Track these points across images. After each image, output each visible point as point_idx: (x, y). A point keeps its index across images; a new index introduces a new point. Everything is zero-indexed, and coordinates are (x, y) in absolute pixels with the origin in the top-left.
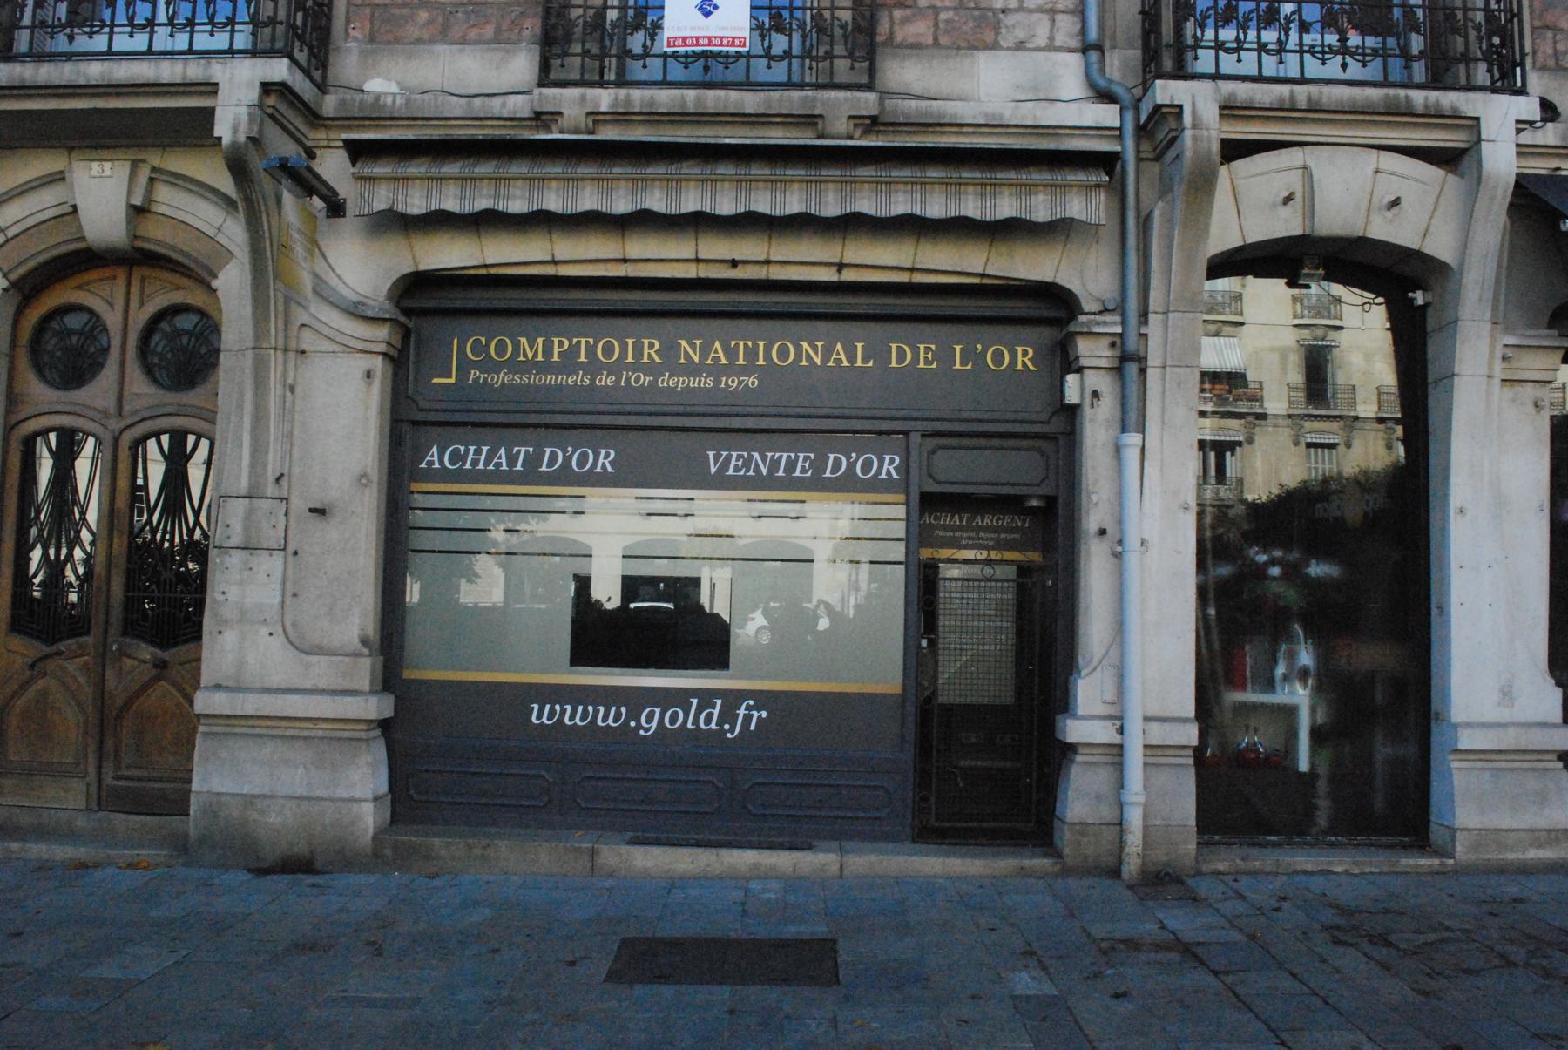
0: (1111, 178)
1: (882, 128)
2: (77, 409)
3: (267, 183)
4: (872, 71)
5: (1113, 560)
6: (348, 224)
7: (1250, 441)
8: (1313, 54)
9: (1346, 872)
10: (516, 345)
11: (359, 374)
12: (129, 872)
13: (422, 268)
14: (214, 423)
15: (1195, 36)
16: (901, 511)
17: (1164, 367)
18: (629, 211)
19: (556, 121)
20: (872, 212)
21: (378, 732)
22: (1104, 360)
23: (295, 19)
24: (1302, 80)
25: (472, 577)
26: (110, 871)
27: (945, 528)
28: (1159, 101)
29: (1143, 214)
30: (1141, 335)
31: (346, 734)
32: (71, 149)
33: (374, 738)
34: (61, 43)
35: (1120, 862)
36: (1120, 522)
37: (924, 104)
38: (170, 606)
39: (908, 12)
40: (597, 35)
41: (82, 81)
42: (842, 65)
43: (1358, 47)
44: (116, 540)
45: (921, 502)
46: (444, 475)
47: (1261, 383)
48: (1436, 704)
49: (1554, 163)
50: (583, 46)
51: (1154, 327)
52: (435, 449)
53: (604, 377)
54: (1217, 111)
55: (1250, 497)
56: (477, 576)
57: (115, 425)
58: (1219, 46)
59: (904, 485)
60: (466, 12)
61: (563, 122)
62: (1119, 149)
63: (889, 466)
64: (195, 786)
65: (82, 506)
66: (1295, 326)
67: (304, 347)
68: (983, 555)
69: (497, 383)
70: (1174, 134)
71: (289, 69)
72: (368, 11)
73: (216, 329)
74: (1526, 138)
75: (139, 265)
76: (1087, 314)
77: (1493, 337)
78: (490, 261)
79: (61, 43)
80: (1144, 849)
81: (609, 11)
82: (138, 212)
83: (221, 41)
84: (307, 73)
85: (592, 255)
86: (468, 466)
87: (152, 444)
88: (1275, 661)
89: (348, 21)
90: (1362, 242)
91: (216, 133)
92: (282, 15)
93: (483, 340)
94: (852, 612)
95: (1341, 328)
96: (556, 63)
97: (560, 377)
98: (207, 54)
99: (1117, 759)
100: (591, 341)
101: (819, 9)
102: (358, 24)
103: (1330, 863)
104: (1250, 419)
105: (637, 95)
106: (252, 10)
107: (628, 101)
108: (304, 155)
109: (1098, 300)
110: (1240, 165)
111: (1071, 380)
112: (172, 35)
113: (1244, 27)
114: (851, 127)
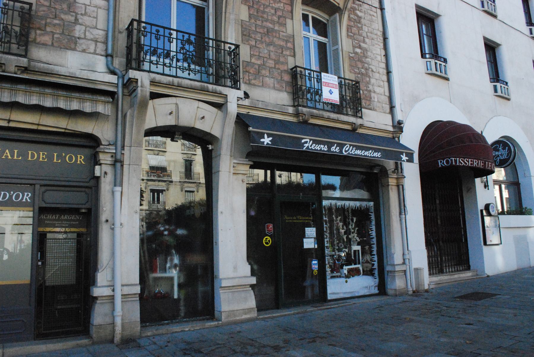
0: (113, 101)
1: (29, 72)
4: (26, 51)
5: (111, 231)
7: (168, 190)
8: (180, 69)
9: (189, 330)
15: (143, 57)
16: (31, 214)
17: (129, 165)
20: (23, 102)
22: (109, 161)
24: (176, 77)
27: (49, 220)
28: (130, 77)
29: (124, 113)
30: (122, 153)
35: (114, 337)
36: (113, 217)
37: (46, 65)
39: (43, 32)
42: (14, 47)
43: (193, 69)
45: (39, 211)
47: (171, 171)
48: (215, 274)
49: (248, 111)
51: (126, 151)
54: (149, 82)
55: (167, 208)
58: (151, 62)
59: (32, 204)
62: (116, 90)
63: (27, 197)
66: (182, 153)
68: (63, 230)
70: (135, 88)
74: (240, 102)
76: (103, 145)
77: (230, 160)
80: (122, 331)
88: (166, 262)
90: (193, 128)
94: (18, 251)
95: (196, 155)
99: (112, 300)
101: (7, 24)
103: (184, 328)
104: (168, 182)
109: (107, 141)
110: (157, 101)
111: (97, 167)
113: (159, 57)
114: (16, 70)
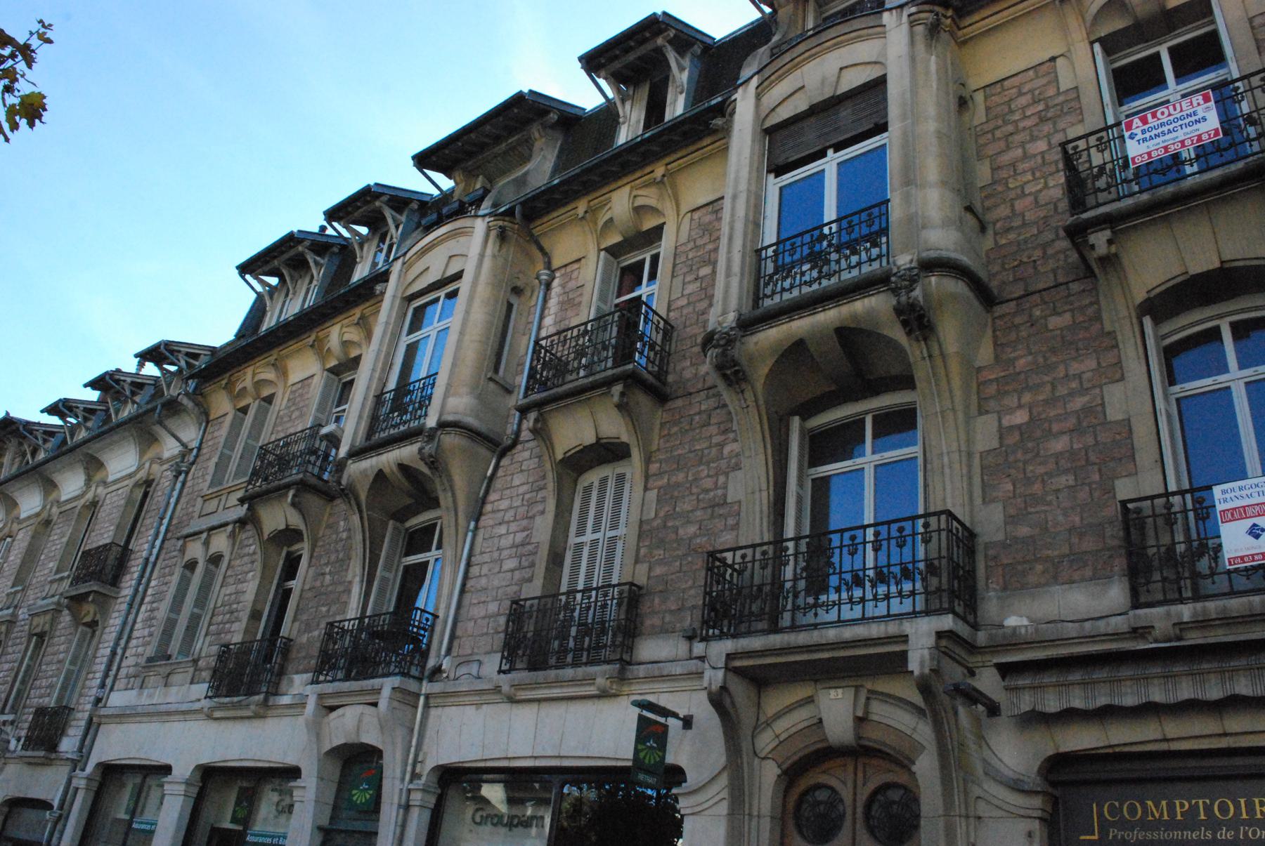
6: (1003, 720)
13: (1063, 749)
32: (816, 681)
34: (810, 619)
50: (1162, 573)
67: (981, 815)
71: (954, 621)
73: (916, 800)
79: (810, 619)
81: (1177, 546)
82: (860, 721)
84: (964, 619)
85: (1197, 732)
89: (987, 579)
91: (910, 669)
93: (1117, 804)
96: (1142, 590)
98: (900, 617)
105: (1212, 606)
107: (1204, 610)
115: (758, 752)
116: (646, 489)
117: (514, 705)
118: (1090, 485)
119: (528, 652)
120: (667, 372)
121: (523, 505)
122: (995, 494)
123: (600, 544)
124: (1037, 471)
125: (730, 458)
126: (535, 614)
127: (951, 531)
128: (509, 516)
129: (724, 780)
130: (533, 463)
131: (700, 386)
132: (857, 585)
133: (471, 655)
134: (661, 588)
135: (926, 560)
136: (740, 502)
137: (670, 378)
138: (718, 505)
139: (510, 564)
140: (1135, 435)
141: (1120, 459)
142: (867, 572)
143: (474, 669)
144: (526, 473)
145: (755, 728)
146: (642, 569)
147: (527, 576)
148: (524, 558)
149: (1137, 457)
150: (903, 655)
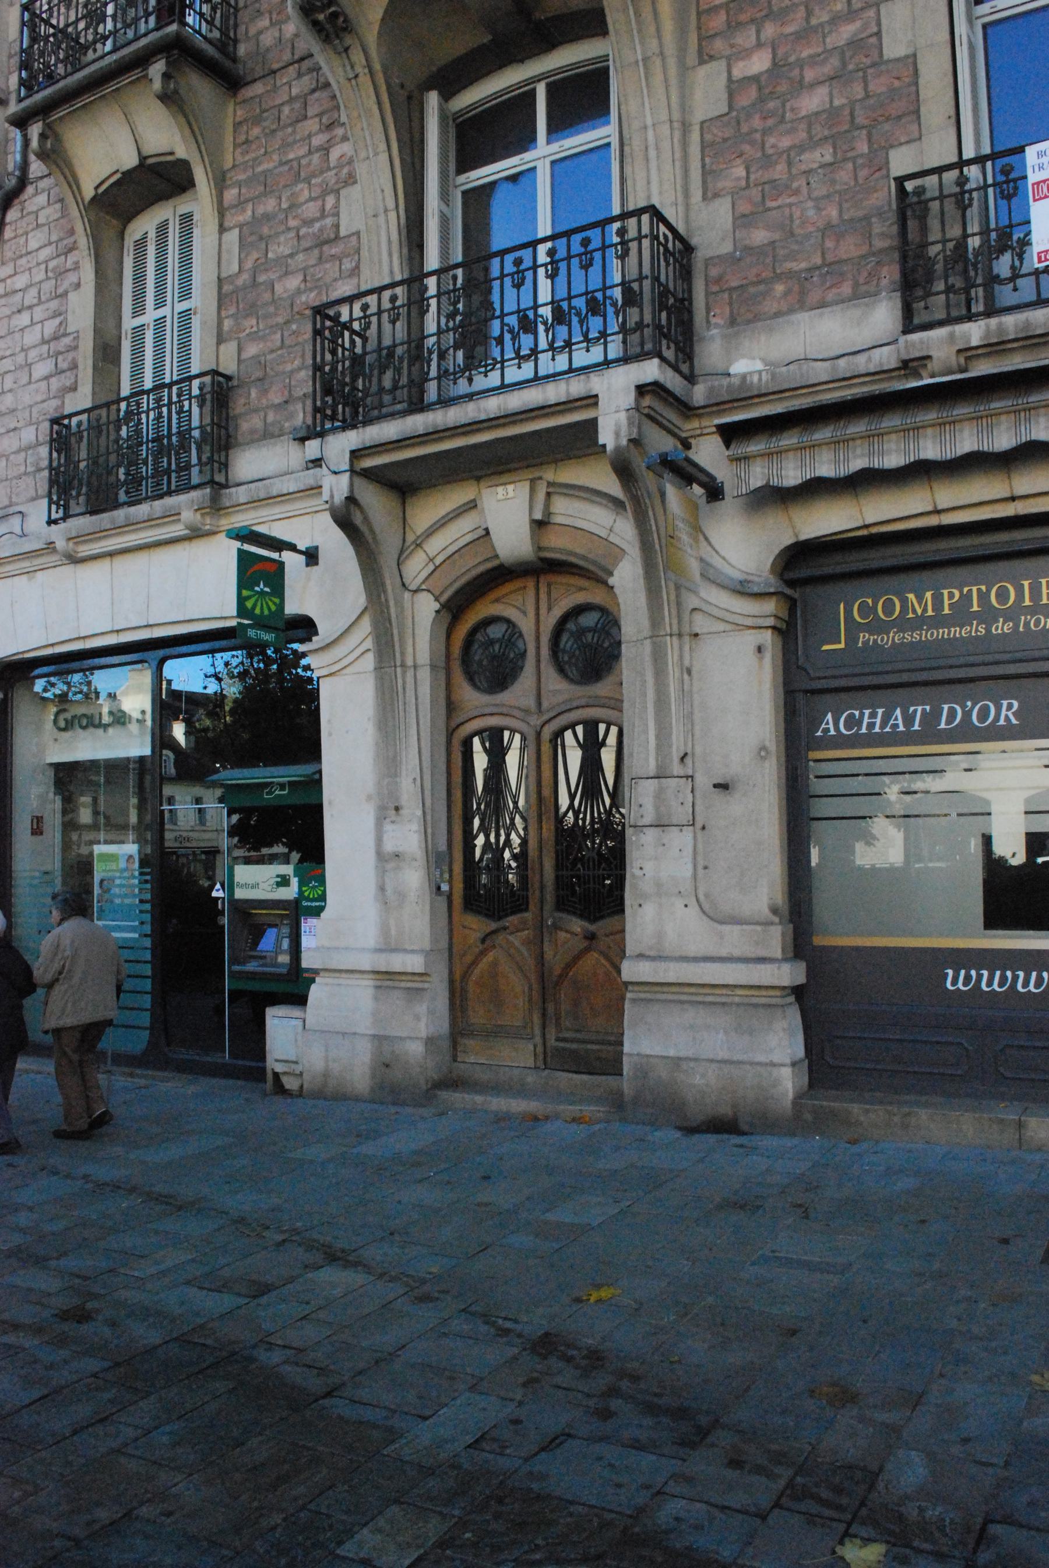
2: (505, 710)
3: (649, 480)
6: (728, 505)
10: (904, 602)
11: (751, 649)
12: (574, 1126)
13: (803, 537)
14: (621, 711)
18: (1014, 445)
19: (926, 365)
21: (792, 999)
23: (660, 320)
25: (869, 839)
26: (558, 1123)
31: (763, 1001)
32: (478, 479)
33: (790, 1004)
34: (462, 387)
38: (594, 883)
40: (959, 267)
41: (483, 417)
44: (544, 826)
46: (840, 741)
52: (829, 716)
53: (1000, 625)
56: (874, 838)
57: (536, 721)
60: (821, 275)
61: (934, 366)
64: (627, 1048)
65: (515, 797)
67: (697, 630)
69: (887, 643)
71: (660, 366)
72: (726, 295)
73: (616, 623)
75: (545, 573)
78: (870, 520)
81: (970, 240)
82: (540, 525)
83: (596, 354)
84: (676, 369)
86: (864, 730)
87: (568, 735)
89: (708, 310)
92: (648, 318)
93: (870, 601)
97: (953, 630)
100: (983, 588)
102: (718, 311)
105: (1010, 321)
106: (620, 320)
107: (1000, 326)
108: (680, 446)
112: (553, 359)
115: (407, 581)
116: (222, 229)
117: (79, 566)
118: (854, 159)
119: (84, 490)
120: (236, 41)
121: (48, 278)
122: (720, 185)
123: (168, 323)
124: (780, 145)
125: (340, 166)
126: (85, 434)
127: (657, 238)
128: (30, 297)
129: (366, 626)
130: (52, 212)
131: (287, 57)
132: (526, 332)
133: (10, 506)
134: (259, 374)
135: (623, 284)
136: (358, 233)
137: (242, 50)
138: (327, 242)
139: (42, 369)
140: (921, 81)
141: (899, 118)
142: (541, 311)
143: (15, 523)
144: (46, 228)
145: (402, 552)
146: (229, 350)
147: (68, 384)
148: (60, 358)
149: (923, 110)
150: (592, 425)
